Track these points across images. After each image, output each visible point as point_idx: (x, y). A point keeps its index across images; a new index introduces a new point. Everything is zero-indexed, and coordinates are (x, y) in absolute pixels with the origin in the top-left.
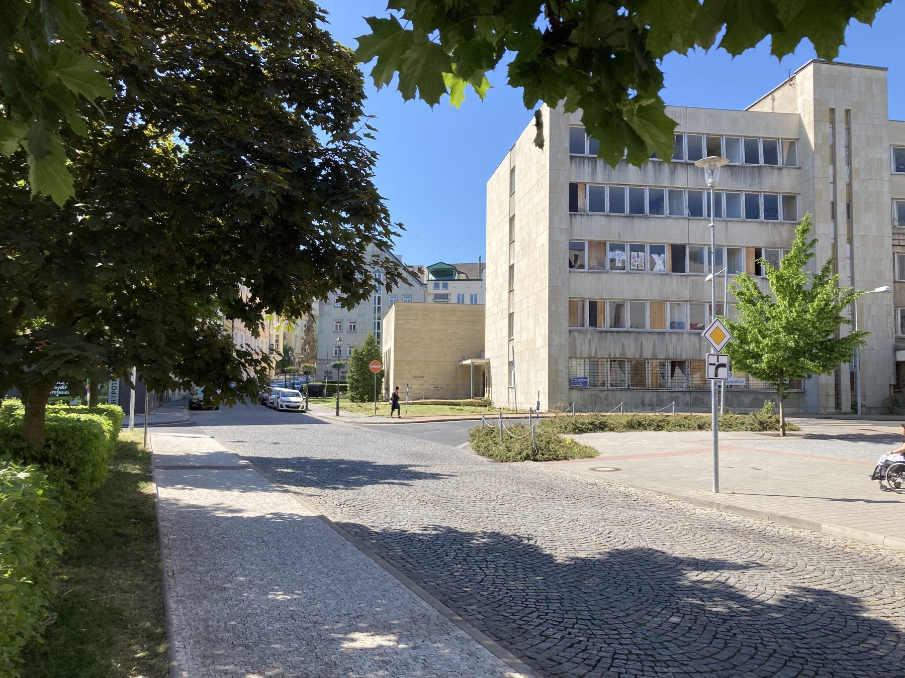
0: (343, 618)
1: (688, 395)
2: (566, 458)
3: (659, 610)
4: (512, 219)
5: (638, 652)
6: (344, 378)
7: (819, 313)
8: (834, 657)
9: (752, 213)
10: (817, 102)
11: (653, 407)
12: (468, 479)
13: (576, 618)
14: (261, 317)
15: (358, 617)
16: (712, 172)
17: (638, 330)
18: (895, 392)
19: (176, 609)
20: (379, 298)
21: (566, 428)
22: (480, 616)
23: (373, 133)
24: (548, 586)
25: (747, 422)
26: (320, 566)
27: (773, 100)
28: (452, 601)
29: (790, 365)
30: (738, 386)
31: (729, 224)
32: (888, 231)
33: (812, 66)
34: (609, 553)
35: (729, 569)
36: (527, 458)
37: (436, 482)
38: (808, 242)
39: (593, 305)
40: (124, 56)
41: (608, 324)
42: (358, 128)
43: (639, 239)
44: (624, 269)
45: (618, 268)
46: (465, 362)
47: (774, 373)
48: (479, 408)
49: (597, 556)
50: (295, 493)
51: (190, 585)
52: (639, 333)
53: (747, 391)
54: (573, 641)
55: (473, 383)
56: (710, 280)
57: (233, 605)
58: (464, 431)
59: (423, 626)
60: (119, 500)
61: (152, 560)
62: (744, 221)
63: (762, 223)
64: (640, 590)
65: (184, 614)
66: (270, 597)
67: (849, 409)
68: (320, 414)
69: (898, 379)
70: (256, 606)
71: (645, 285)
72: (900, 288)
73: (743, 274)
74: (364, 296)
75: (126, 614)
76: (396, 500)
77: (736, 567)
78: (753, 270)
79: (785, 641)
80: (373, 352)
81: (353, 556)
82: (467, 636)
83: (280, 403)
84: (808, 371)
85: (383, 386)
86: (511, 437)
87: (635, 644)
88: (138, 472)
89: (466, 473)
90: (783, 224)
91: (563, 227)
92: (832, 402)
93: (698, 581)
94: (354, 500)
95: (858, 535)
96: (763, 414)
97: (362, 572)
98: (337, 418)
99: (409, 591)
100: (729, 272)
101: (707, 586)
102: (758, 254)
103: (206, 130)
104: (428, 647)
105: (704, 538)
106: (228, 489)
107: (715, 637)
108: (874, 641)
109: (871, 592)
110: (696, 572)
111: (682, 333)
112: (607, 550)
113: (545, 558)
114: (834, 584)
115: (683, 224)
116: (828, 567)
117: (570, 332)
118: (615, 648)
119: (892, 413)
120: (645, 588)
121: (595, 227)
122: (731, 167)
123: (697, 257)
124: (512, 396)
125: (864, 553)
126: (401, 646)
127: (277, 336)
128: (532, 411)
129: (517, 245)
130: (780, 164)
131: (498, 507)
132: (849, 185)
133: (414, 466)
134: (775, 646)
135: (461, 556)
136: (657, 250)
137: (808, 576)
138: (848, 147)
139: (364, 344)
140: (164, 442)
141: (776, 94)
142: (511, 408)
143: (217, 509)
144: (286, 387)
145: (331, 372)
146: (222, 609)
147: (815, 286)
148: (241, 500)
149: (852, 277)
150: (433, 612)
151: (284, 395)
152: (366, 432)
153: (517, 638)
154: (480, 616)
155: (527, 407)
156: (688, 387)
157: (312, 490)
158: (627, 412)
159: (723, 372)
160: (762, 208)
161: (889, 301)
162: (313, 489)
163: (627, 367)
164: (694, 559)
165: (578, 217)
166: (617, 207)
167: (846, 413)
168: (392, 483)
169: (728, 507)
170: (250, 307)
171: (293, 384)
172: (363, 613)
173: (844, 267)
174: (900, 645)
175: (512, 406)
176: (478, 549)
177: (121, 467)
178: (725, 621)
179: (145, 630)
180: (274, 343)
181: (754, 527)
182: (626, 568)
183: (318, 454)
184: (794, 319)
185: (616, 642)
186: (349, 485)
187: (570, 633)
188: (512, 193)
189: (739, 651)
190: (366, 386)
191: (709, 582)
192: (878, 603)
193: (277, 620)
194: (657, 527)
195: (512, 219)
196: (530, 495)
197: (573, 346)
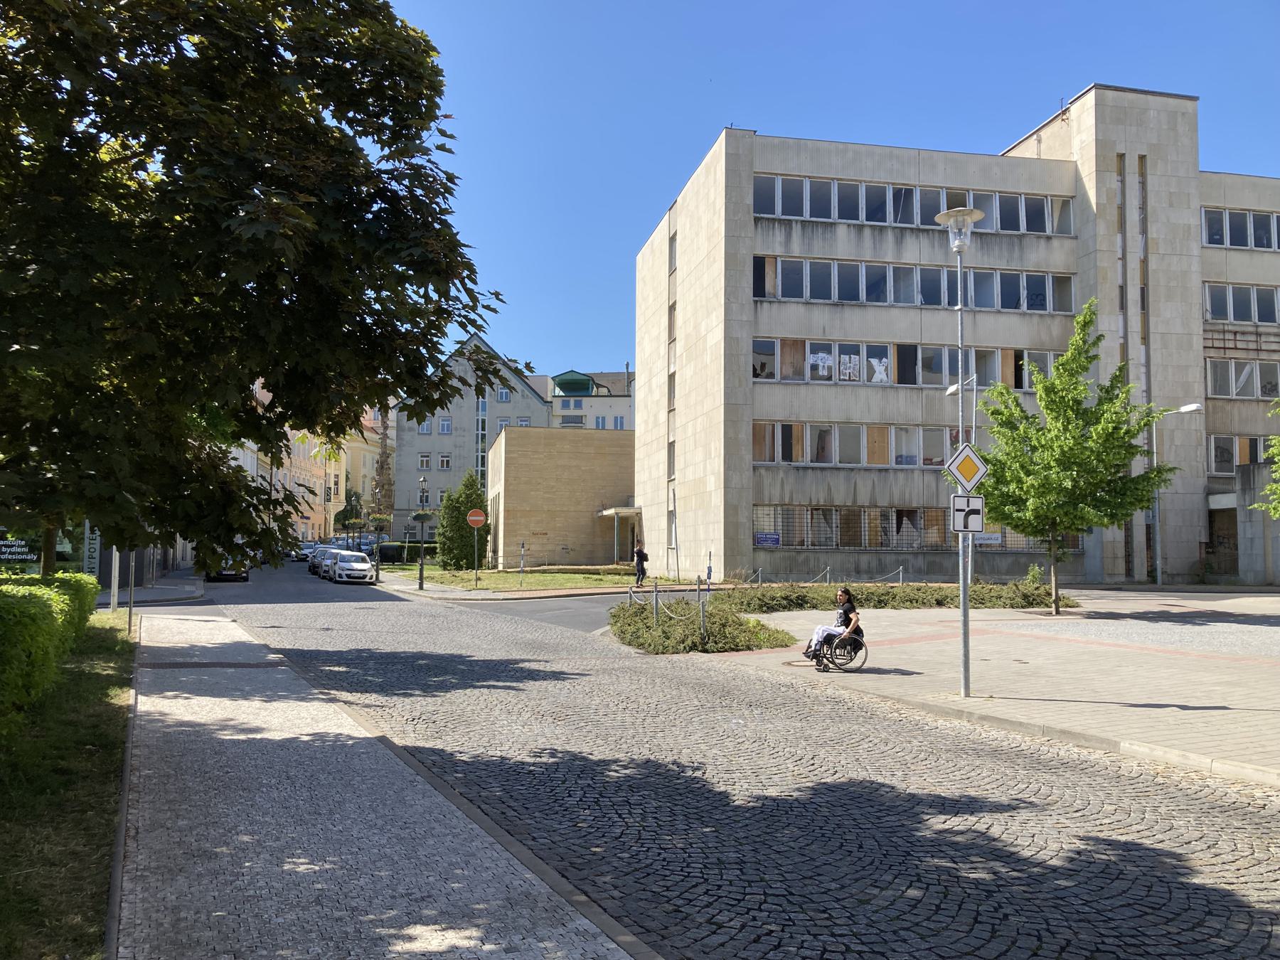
0: (399, 901)
1: (920, 558)
2: (749, 648)
3: (889, 878)
4: (672, 308)
5: (860, 948)
6: (432, 535)
7: (1107, 440)
8: (1159, 951)
9: (1010, 301)
10: (1102, 144)
11: (871, 575)
12: (606, 679)
13: (765, 894)
14: (285, 436)
15: (423, 899)
16: (960, 230)
17: (850, 464)
18: (1208, 553)
19: (132, 891)
20: (483, 421)
21: (749, 604)
22: (616, 893)
23: (449, 143)
24: (721, 842)
25: (1004, 594)
26: (373, 816)
27: (1039, 141)
28: (574, 871)
29: (1066, 514)
30: (987, 546)
31: (979, 316)
32: (1197, 327)
33: (1093, 93)
34: (812, 788)
35: (991, 811)
36: (693, 647)
37: (559, 684)
38: (1091, 340)
39: (787, 430)
40: (53, 16)
41: (808, 457)
42: (430, 138)
43: (852, 337)
44: (829, 378)
45: (822, 378)
46: (605, 513)
47: (1043, 526)
48: (626, 578)
49: (795, 794)
50: (346, 702)
51: (160, 851)
52: (852, 470)
53: (1003, 552)
54: (759, 931)
55: (621, 544)
56: (954, 394)
57: (226, 883)
58: (603, 610)
59: (525, 912)
60: (73, 716)
61: (104, 811)
62: (999, 312)
63: (1024, 314)
64: (861, 847)
65: (143, 900)
66: (287, 867)
67: (1144, 577)
68: (396, 587)
69: (1211, 535)
70: (262, 883)
71: (860, 402)
72: (1214, 407)
73: (1000, 386)
74: (442, 403)
75: (45, 901)
76: (497, 712)
77: (998, 808)
78: (1012, 381)
79: (1082, 924)
80: (474, 497)
81: (425, 799)
82: (593, 929)
83: (338, 572)
84: (1096, 525)
85: (489, 548)
86: (671, 618)
87: (855, 935)
88: (111, 672)
89: (604, 671)
90: (1052, 316)
91: (745, 318)
92: (1121, 566)
93: (946, 831)
94: (435, 712)
95: (1174, 756)
96: (1028, 584)
97: (436, 825)
98: (421, 593)
99: (507, 855)
100: (979, 383)
101: (959, 839)
102: (1018, 356)
103: (186, 135)
104: (530, 949)
105: (951, 764)
106: (246, 696)
107: (976, 921)
108: (1214, 923)
109: (1201, 845)
110: (943, 817)
111: (912, 470)
112: (810, 784)
113: (718, 798)
114: (1147, 833)
115: (913, 315)
116: (1135, 806)
117: (755, 468)
118: (825, 942)
119: (1203, 582)
120: (869, 843)
121: (788, 319)
122: (981, 234)
123: (932, 365)
124: (672, 561)
125: (1184, 785)
126: (488, 947)
127: (337, 476)
128: (700, 582)
129: (679, 345)
130: (1049, 231)
131: (649, 720)
132: (1145, 262)
133: (529, 661)
134: (1068, 934)
135: (591, 796)
136: (877, 352)
137: (1107, 821)
138: (1143, 208)
139: (461, 487)
140: (160, 628)
141: (1042, 133)
142: (671, 577)
143: (224, 728)
144: (348, 548)
145: (414, 528)
146: (207, 890)
147: (1100, 403)
148: (263, 713)
149: (1148, 391)
150: (544, 889)
151: (344, 559)
152: (461, 612)
153: (672, 929)
154: (616, 893)
155: (693, 576)
156: (921, 547)
157: (372, 698)
158: (836, 581)
159: (975, 522)
160: (1024, 293)
161: (1199, 424)
162: (374, 696)
163: (836, 519)
164: (939, 797)
165: (766, 305)
166: (821, 290)
167: (1140, 583)
168: (494, 687)
169: (984, 718)
170: (268, 419)
171: (359, 545)
172: (433, 892)
173: (1138, 378)
174: (1254, 928)
175: (672, 575)
176: (618, 785)
177: (86, 667)
178: (990, 894)
179: (72, 928)
180: (332, 486)
181: (1023, 747)
182: (839, 811)
183: (387, 645)
184: (1071, 449)
185: (826, 931)
186: (428, 690)
187: (754, 919)
188: (672, 271)
189: (1014, 943)
190: (466, 547)
191: (962, 833)
192: (1214, 861)
193: (292, 907)
194: (883, 748)
195: (672, 308)
196: (696, 703)
197: (758, 489)
